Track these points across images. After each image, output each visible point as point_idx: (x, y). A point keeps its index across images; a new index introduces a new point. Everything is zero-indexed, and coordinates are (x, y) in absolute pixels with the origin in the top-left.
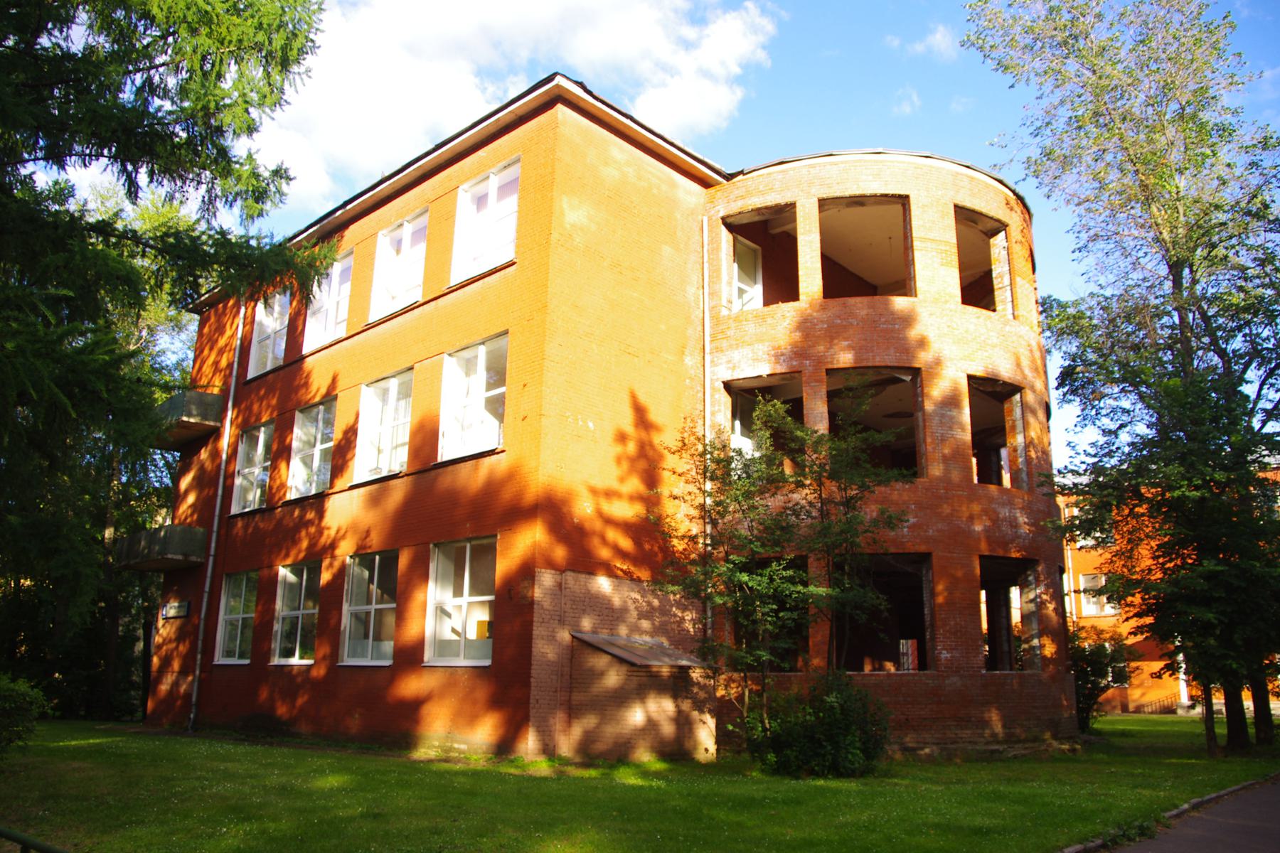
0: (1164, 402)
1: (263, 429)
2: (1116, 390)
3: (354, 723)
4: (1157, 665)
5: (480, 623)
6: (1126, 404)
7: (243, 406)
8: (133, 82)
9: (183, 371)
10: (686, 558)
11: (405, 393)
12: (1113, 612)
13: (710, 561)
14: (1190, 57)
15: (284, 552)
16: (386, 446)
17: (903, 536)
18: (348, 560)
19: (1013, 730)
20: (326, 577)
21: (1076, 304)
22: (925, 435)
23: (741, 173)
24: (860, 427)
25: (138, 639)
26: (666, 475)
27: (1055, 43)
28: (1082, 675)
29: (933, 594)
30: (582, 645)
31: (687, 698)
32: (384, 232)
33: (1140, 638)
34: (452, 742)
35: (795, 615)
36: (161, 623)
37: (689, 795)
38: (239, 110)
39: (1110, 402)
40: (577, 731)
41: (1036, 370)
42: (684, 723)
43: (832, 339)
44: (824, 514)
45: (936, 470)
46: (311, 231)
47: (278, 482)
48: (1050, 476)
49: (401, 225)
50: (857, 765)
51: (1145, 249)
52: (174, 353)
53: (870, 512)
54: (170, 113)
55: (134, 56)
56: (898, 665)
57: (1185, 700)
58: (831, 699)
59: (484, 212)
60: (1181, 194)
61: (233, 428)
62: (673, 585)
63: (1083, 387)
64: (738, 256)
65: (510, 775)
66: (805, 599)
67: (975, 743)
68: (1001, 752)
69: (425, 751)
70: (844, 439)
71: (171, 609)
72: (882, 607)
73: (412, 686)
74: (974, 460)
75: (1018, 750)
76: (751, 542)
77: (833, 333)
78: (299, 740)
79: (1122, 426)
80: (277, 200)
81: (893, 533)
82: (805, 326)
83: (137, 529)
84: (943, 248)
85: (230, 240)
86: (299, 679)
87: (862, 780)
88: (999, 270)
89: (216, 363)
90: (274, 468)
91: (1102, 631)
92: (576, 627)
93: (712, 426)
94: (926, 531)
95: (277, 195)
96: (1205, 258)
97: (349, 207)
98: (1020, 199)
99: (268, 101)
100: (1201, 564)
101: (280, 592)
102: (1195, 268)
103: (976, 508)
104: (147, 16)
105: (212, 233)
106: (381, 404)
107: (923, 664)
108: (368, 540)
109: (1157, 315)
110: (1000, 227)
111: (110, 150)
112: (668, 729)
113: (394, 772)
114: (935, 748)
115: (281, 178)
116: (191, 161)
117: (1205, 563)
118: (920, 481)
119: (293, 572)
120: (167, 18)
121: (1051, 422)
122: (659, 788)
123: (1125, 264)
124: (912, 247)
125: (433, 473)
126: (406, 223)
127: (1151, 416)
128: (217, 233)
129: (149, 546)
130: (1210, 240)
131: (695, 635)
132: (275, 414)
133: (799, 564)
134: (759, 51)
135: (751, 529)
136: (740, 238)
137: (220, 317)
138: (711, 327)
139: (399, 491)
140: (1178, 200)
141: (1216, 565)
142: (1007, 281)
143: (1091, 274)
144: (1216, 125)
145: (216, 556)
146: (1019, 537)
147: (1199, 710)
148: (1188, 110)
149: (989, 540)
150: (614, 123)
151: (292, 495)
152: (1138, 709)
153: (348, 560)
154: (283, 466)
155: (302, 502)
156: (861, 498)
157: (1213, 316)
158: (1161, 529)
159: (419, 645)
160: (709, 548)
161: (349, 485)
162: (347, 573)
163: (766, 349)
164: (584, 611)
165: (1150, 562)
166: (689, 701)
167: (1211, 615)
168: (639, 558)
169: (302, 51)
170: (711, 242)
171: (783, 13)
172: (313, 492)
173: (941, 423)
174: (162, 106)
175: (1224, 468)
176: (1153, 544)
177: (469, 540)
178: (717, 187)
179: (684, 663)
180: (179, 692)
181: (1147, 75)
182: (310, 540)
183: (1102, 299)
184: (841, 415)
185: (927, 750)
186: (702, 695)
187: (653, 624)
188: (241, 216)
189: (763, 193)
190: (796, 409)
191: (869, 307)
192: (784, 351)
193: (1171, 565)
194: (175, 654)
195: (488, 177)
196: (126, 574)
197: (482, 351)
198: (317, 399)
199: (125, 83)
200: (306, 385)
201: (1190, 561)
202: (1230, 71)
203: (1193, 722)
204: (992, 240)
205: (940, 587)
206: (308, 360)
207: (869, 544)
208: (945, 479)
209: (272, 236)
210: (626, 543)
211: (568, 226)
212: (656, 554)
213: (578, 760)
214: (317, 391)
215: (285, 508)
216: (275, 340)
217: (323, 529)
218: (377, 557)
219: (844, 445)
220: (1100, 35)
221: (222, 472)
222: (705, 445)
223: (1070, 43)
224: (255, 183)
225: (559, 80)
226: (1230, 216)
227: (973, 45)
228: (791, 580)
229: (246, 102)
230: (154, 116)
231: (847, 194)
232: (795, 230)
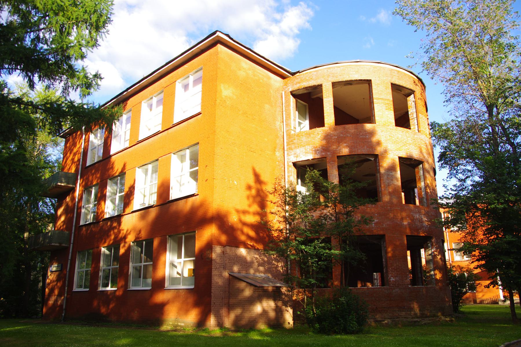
0: (486, 166)
1: (94, 188)
2: (465, 162)
3: (135, 315)
4: (488, 282)
5: (189, 270)
6: (469, 168)
7: (85, 177)
8: (30, 37)
9: (59, 163)
10: (278, 239)
11: (155, 171)
12: (467, 259)
13: (288, 241)
14: (495, 15)
15: (103, 241)
16: (147, 194)
17: (372, 228)
18: (132, 244)
19: (424, 312)
20: (122, 251)
21: (446, 125)
22: (381, 183)
23: (298, 72)
24: (351, 181)
25: (40, 282)
26: (269, 203)
27: (434, 11)
28: (454, 287)
29: (386, 253)
30: (233, 278)
31: (280, 300)
32: (144, 101)
33: (479, 270)
34: (178, 322)
35: (325, 263)
36: (49, 274)
37: (280, 343)
38: (77, 48)
39: (462, 167)
40: (232, 316)
41: (429, 154)
42: (279, 312)
43: (339, 143)
44: (337, 219)
45: (386, 198)
46: (113, 101)
47: (101, 210)
48: (436, 200)
49: (152, 98)
50: (354, 329)
51: (476, 100)
52: (54, 155)
53: (357, 217)
54: (46, 50)
55: (30, 25)
56: (373, 284)
57: (502, 298)
58: (342, 299)
59: (187, 92)
60: (491, 75)
61: (81, 187)
62: (272, 251)
63: (450, 161)
64: (298, 108)
65: (202, 336)
66: (330, 255)
67: (407, 318)
68: (419, 322)
69: (165, 327)
70: (345, 186)
71: (54, 268)
72: (364, 259)
73: (160, 297)
74: (403, 194)
75: (426, 321)
76: (306, 232)
77: (340, 140)
79: (467, 177)
80: (96, 88)
81: (368, 227)
82: (327, 137)
83: (39, 232)
85: (74, 105)
86: (111, 297)
87: (357, 335)
88: (412, 111)
89: (73, 159)
91: (463, 267)
92: (231, 270)
93: (288, 182)
94: (382, 225)
95: (96, 86)
96: (503, 103)
97: (129, 91)
98: (420, 80)
99: (90, 44)
100: (505, 237)
101: (102, 258)
102: (498, 107)
103: (404, 214)
104: (35, 7)
105: (67, 102)
106: (145, 176)
107: (383, 283)
108: (140, 234)
109: (482, 129)
110: (412, 92)
111: (21, 67)
112: (272, 314)
113: (151, 336)
114: (389, 320)
115: (98, 78)
116: (57, 71)
117: (507, 237)
118: (379, 204)
119: (108, 249)
120: (44, 8)
121: (436, 176)
122: (267, 340)
123: (467, 107)
124: (373, 102)
125: (168, 205)
126: (154, 97)
127: (481, 173)
128: (69, 102)
129: (44, 240)
130: (505, 95)
132: (99, 181)
133: (327, 241)
134: (307, 23)
135: (305, 226)
136: (299, 100)
137: (74, 139)
138: (287, 139)
139: (153, 213)
141: (512, 237)
142: (415, 116)
143: (452, 112)
144: (507, 44)
145: (73, 244)
146: (423, 227)
147: (508, 302)
148: (494, 38)
149: (411, 229)
150: (243, 52)
151: (107, 216)
152: (482, 302)
153: (132, 244)
154: (103, 203)
155: (111, 219)
156: (353, 212)
157: (507, 128)
158: (487, 222)
159: (163, 280)
160: (288, 235)
161: (131, 211)
162: (131, 249)
163: (311, 148)
164: (234, 264)
165: (482, 237)
166: (281, 302)
167: (511, 260)
168: (258, 240)
169: (105, 23)
170: (286, 102)
171: (317, 7)
172: (116, 214)
173: (388, 178)
174: (43, 47)
175: (514, 195)
176: (484, 229)
177: (184, 234)
179: (278, 285)
180: (57, 304)
181: (475, 24)
182: (115, 235)
183: (457, 122)
184: (343, 176)
185: (386, 322)
186: (286, 299)
187: (265, 268)
188: (80, 95)
189: (308, 81)
190: (324, 174)
191: (355, 129)
192: (319, 149)
193: (492, 237)
194: (56, 287)
195: (189, 77)
196: (34, 253)
197: (188, 152)
198: (117, 174)
199: (26, 37)
200: (112, 168)
201: (500, 236)
202: (513, 20)
203: (506, 307)
204: (408, 98)
205: (389, 249)
206: (113, 157)
207: (357, 231)
208: (390, 202)
209: (94, 103)
210: (252, 233)
212: (265, 238)
213: (233, 329)
214: (117, 170)
215: (104, 222)
216: (98, 148)
217: (121, 230)
218: (144, 242)
219: (345, 189)
220: (454, 7)
221: (76, 207)
222: (285, 190)
223: (440, 11)
224: (86, 80)
225: (218, 34)
226: (513, 84)
227: (398, 13)
228: (324, 248)
229: (80, 45)
230: (39, 51)
231: (344, 80)
232: (322, 96)
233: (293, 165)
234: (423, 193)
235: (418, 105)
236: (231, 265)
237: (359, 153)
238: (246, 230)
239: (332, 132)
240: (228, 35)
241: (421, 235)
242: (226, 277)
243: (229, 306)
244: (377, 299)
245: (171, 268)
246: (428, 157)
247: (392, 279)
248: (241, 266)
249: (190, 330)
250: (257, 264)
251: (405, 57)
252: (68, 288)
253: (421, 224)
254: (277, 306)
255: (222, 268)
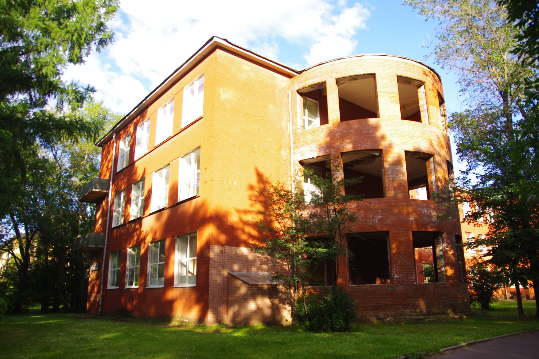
3: (152, 311)
7: (116, 183)
15: (129, 242)
19: (431, 309)
20: (142, 251)
29: (391, 249)
31: (276, 298)
32: (160, 108)
36: (91, 272)
40: (231, 312)
41: (442, 146)
42: (275, 309)
43: (343, 139)
45: (390, 193)
46: (135, 110)
47: (127, 213)
64: (305, 106)
68: (423, 319)
69: (175, 323)
73: (171, 294)
75: (431, 318)
77: (343, 136)
78: (133, 319)
80: (90, 100)
82: (331, 134)
84: (392, 95)
89: (107, 166)
90: (126, 207)
94: (386, 221)
97: (147, 99)
103: (410, 209)
112: (268, 312)
114: (391, 317)
126: (167, 104)
131: (289, 270)
132: (126, 185)
137: (109, 147)
140: (504, 64)
145: (107, 245)
149: (417, 224)
151: (132, 219)
153: (149, 244)
154: (129, 206)
163: (315, 146)
164: (234, 262)
166: (278, 299)
167: (514, 254)
168: (262, 239)
177: (189, 234)
178: (295, 78)
182: (137, 236)
185: (388, 319)
186: (284, 296)
198: (139, 179)
200: (136, 173)
208: (395, 197)
210: (254, 232)
211: (223, 100)
213: (231, 325)
218: (159, 243)
225: (215, 39)
231: (348, 75)
233: (300, 163)
234: (434, 187)
235: (428, 96)
236: (231, 264)
237: (363, 149)
238: (247, 229)
239: (335, 129)
240: (225, 40)
241: (430, 230)
242: (225, 276)
243: (228, 304)
244: (380, 296)
245: (180, 267)
246: (440, 150)
247: (396, 276)
248: (242, 265)
249: (191, 326)
250: (259, 262)
251: (420, 46)
252: (103, 286)
253: (429, 219)
254: (273, 304)
255: (221, 267)
